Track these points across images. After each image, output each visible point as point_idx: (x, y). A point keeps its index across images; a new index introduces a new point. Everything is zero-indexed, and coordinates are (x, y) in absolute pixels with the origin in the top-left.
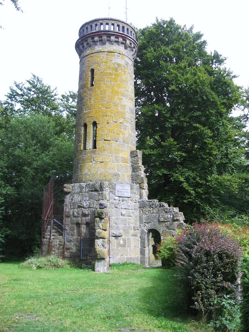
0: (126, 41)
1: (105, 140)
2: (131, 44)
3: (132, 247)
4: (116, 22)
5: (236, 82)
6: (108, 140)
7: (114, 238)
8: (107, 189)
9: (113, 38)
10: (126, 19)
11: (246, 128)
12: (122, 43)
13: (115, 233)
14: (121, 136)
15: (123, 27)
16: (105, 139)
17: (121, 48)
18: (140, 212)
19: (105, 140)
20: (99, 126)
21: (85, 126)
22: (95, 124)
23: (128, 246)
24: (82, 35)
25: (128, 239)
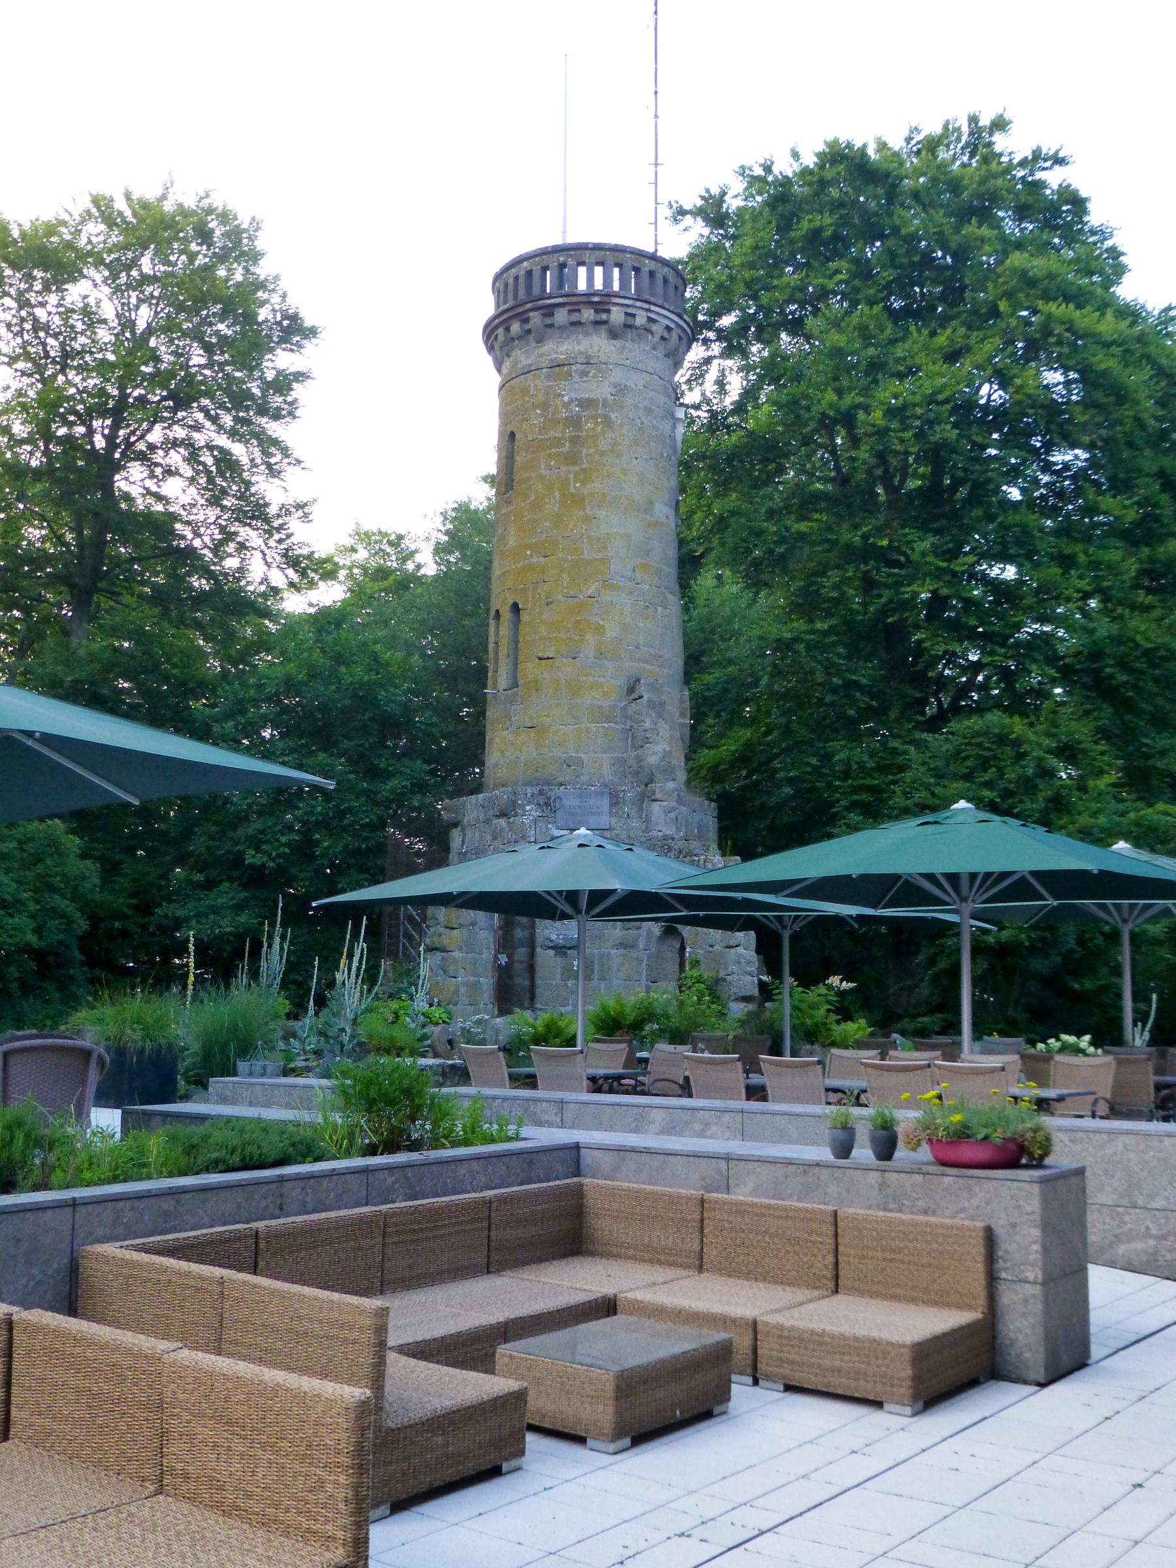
0: (608, 311)
1: (540, 659)
3: (615, 981)
4: (571, 256)
5: (147, 197)
6: (548, 658)
7: (552, 952)
8: (528, 808)
9: (561, 316)
10: (656, 244)
11: (311, 605)
12: (598, 323)
13: (554, 937)
14: (590, 638)
15: (652, 274)
16: (540, 655)
17: (598, 344)
19: (540, 659)
20: (525, 617)
22: (516, 608)
23: (602, 978)
25: (601, 956)
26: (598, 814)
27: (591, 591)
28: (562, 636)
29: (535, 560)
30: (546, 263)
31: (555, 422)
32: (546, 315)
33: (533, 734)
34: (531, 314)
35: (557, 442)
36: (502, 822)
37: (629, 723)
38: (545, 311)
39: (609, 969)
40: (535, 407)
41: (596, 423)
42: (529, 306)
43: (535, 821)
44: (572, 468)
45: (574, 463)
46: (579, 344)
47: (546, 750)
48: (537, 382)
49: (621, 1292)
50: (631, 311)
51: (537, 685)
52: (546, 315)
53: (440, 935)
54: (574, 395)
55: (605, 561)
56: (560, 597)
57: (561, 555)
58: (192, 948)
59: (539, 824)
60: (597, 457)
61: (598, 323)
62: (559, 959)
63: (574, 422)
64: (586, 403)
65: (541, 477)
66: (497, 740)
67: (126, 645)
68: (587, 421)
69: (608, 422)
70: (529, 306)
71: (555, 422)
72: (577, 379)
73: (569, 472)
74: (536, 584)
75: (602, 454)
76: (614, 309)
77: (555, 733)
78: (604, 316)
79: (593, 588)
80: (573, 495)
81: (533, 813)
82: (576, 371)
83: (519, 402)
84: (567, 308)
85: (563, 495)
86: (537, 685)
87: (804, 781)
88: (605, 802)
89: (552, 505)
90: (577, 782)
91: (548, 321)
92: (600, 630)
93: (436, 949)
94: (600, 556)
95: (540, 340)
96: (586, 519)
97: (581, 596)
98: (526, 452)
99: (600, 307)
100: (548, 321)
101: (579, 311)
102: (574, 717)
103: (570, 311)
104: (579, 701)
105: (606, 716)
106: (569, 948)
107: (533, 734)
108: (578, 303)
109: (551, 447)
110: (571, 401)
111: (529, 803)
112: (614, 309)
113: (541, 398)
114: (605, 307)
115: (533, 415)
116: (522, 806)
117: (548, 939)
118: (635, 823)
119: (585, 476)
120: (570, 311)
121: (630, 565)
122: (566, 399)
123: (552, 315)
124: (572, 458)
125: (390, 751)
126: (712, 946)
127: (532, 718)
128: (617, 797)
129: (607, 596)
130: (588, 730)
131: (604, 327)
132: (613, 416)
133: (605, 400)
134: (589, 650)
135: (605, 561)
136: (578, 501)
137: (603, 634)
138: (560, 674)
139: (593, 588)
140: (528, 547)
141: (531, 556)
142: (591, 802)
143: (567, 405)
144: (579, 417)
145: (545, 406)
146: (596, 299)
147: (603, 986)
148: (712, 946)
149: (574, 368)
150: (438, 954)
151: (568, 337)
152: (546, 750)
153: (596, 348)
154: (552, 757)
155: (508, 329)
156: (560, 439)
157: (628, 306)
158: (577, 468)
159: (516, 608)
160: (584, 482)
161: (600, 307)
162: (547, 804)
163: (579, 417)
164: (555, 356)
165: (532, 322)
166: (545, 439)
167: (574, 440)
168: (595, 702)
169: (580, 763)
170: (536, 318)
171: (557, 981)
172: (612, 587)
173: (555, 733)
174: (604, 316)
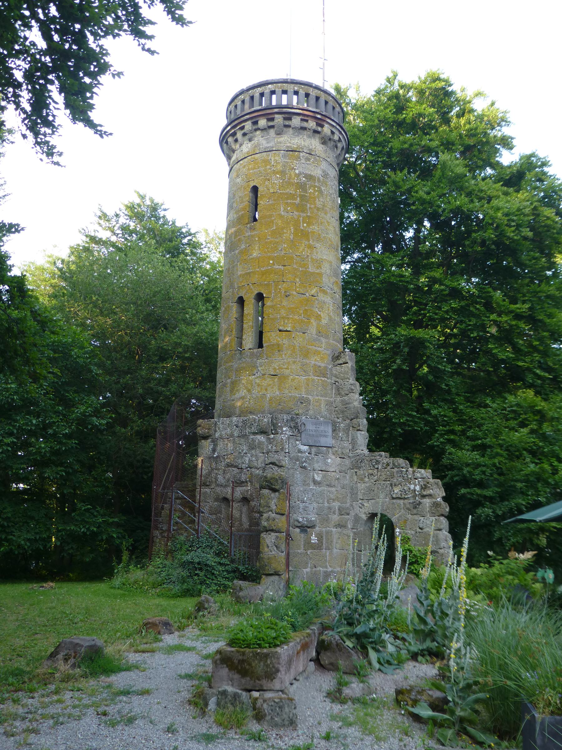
0: (322, 126)
1: (280, 331)
2: (333, 133)
3: (335, 551)
7: (298, 530)
8: (284, 429)
12: (316, 132)
13: (301, 520)
16: (281, 328)
18: (351, 477)
19: (280, 331)
20: (268, 303)
21: (241, 301)
22: (260, 297)
23: (328, 548)
24: (233, 117)
25: (327, 533)
26: (326, 436)
27: (313, 292)
28: (296, 317)
29: (276, 267)
30: (285, 89)
31: (289, 184)
32: (285, 119)
33: (276, 380)
34: (276, 116)
35: (292, 197)
36: (261, 438)
37: (334, 378)
38: (286, 116)
39: (332, 542)
40: (275, 173)
41: (315, 190)
42: (276, 110)
43: (288, 438)
44: (302, 214)
45: (303, 211)
46: (304, 141)
47: (287, 391)
48: (277, 158)
49: (209, 738)
50: (334, 130)
51: (279, 348)
52: (285, 119)
53: (274, 520)
54: (301, 170)
55: (320, 275)
56: (294, 293)
57: (295, 266)
58: (408, 562)
59: (291, 441)
60: (315, 211)
61: (316, 132)
62: (302, 535)
63: (302, 186)
64: (310, 177)
65: (281, 216)
66: (243, 382)
67: (355, 193)
68: (310, 188)
69: (320, 192)
70: (276, 110)
71: (289, 184)
72: (303, 161)
73: (300, 216)
74: (277, 283)
75: (318, 209)
76: (326, 126)
77: (293, 380)
78: (319, 129)
79: (314, 290)
80: (302, 230)
81: (287, 433)
82: (303, 156)
83: (262, 169)
84: (301, 117)
85: (296, 229)
86: (279, 348)
87: (409, 426)
88: (330, 429)
89: (289, 234)
90: (307, 414)
91: (287, 123)
92: (318, 318)
93: (272, 530)
94: (318, 271)
95: (279, 134)
96: (311, 247)
97: (307, 294)
98: (269, 199)
99: (319, 122)
100: (287, 123)
101: (307, 121)
102: (305, 371)
103: (302, 120)
104: (308, 362)
105: (322, 373)
106: (309, 527)
107: (276, 380)
108: (308, 116)
109: (287, 199)
110: (300, 174)
111: (285, 426)
112: (326, 126)
113: (279, 168)
114: (322, 123)
115: (274, 177)
116: (281, 427)
117: (298, 521)
118: (346, 444)
119: (309, 220)
120: (302, 120)
121: (332, 280)
122: (297, 171)
123: (290, 119)
124: (301, 208)
125: (429, 362)
126: (421, 529)
127: (275, 369)
128: (335, 426)
129: (321, 297)
130: (313, 380)
131: (317, 136)
132: (323, 188)
133: (319, 179)
134: (313, 330)
135: (320, 275)
136: (305, 235)
137: (320, 320)
138: (295, 342)
139: (314, 290)
140: (270, 258)
141: (273, 264)
142: (322, 428)
143: (298, 175)
144: (305, 184)
145: (283, 173)
146: (319, 116)
147: (328, 554)
148: (421, 529)
149: (301, 154)
150: (273, 534)
151: (298, 136)
152: (287, 391)
153: (314, 147)
154: (290, 397)
155: (255, 123)
156: (294, 195)
157: (333, 126)
158: (305, 215)
159: (260, 297)
160: (309, 224)
161: (319, 122)
162: (296, 427)
163: (305, 184)
164: (289, 145)
165: (276, 121)
166: (283, 193)
167: (302, 197)
168: (317, 363)
169: (308, 401)
170: (279, 119)
171: (301, 551)
172: (325, 292)
173: (293, 380)
174: (319, 129)
